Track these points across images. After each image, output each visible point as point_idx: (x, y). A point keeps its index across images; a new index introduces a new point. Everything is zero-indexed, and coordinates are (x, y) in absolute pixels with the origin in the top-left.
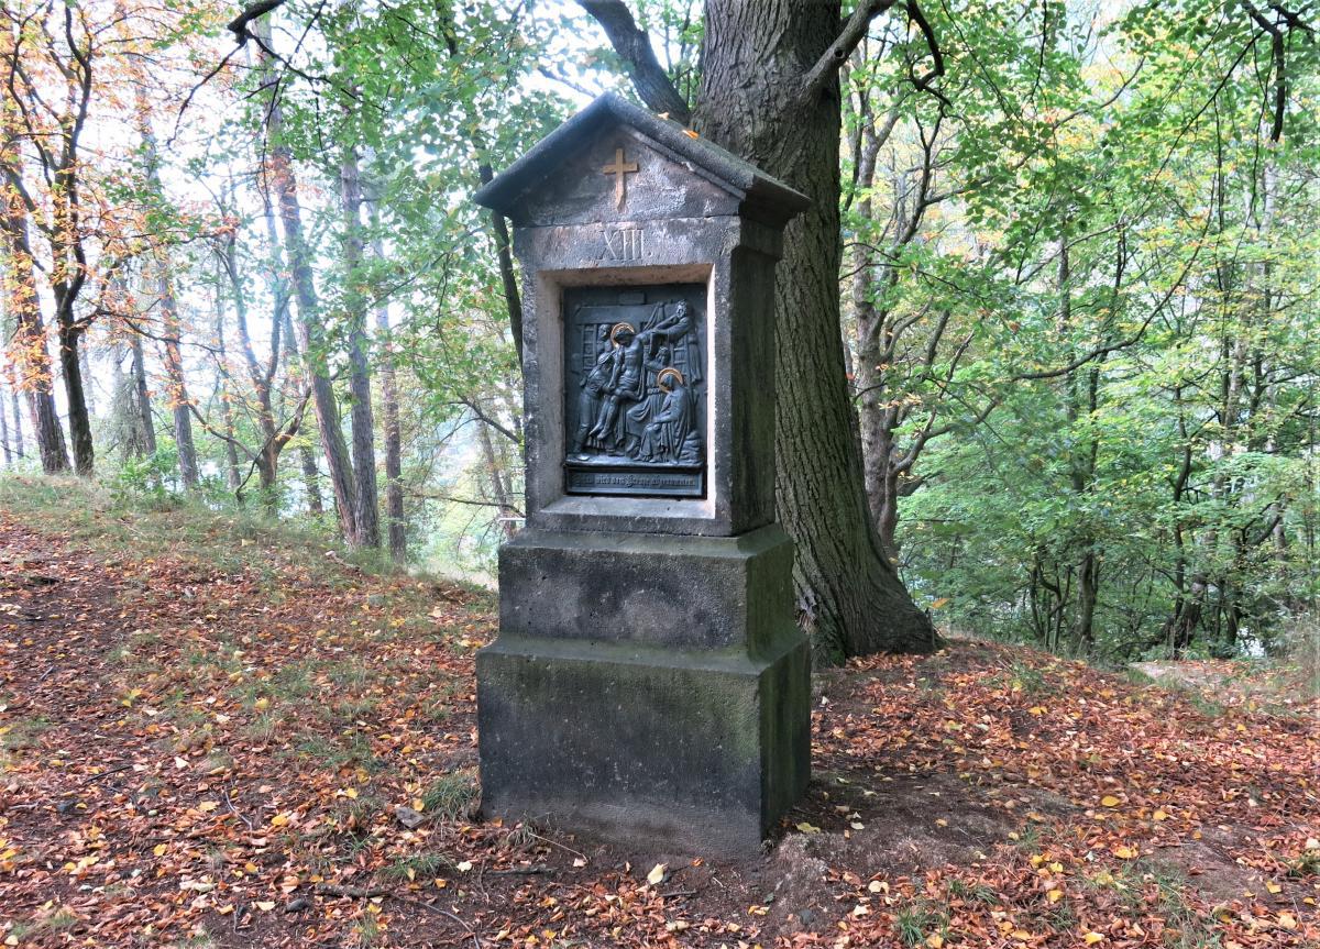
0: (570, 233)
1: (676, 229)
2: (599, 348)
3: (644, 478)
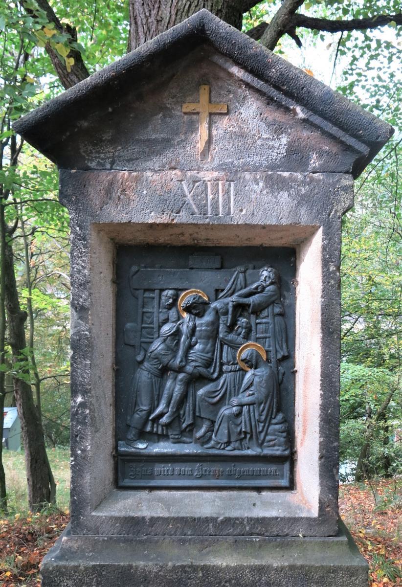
0: (137, 180)
1: (275, 184)
2: (162, 317)
3: (217, 468)
